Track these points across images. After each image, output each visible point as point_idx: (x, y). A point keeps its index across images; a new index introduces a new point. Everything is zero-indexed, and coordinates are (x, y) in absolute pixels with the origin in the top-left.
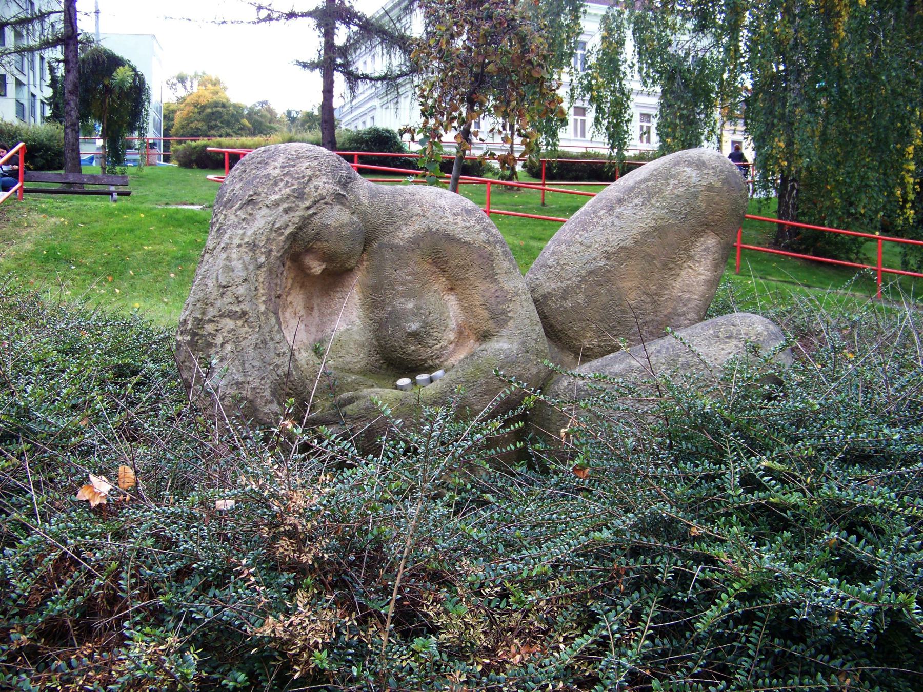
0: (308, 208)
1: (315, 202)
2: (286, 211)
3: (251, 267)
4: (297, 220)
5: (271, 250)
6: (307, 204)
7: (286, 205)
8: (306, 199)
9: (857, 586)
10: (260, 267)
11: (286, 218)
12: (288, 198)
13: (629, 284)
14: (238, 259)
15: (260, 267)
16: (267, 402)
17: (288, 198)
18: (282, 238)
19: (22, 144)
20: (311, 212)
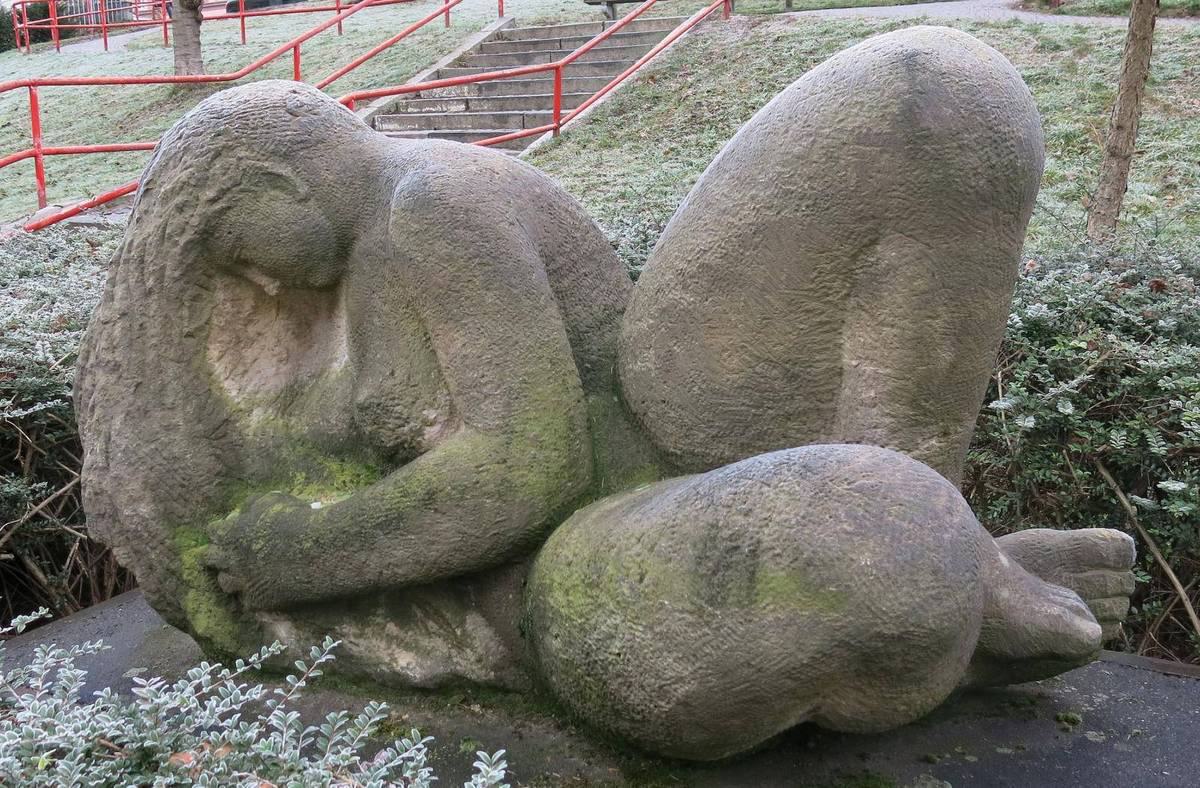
0: (213, 201)
1: (223, 192)
2: (180, 209)
3: (136, 294)
4: (195, 221)
5: (163, 268)
6: (210, 194)
7: (179, 199)
8: (210, 187)
9: (1091, 373)
10: (149, 293)
11: (179, 219)
12: (182, 188)
13: (723, 340)
14: (437, 452)
15: (149, 293)
16: (133, 500)
17: (182, 188)
18: (177, 250)
19: (999, 750)
20: (217, 207)
